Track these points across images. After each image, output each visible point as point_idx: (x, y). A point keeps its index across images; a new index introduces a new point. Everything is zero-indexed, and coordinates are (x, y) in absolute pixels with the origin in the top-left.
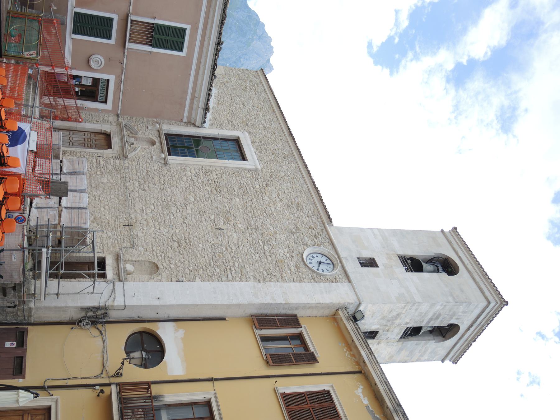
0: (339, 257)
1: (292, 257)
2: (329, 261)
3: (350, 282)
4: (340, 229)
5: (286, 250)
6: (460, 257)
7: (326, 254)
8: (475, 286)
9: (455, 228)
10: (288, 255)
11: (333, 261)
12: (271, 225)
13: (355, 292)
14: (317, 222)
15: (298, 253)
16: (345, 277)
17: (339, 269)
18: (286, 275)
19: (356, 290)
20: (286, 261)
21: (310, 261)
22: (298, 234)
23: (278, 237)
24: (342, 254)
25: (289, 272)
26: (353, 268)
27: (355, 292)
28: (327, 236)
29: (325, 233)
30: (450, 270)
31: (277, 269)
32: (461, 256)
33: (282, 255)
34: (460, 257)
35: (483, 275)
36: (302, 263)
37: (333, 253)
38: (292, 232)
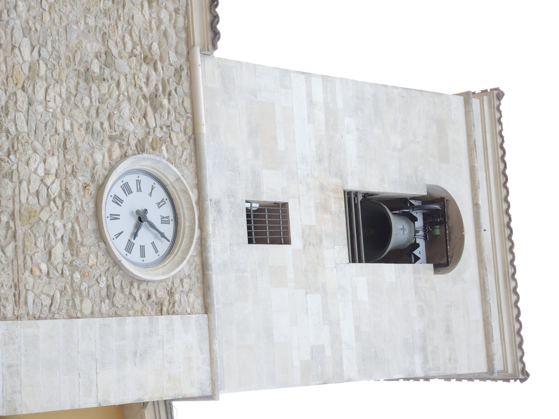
0: (201, 201)
1: (68, 194)
2: (168, 230)
3: (207, 309)
4: (227, 68)
5: (53, 162)
6: (476, 205)
7: (167, 182)
8: (478, 316)
9: (499, 95)
10: (55, 188)
11: (180, 212)
12: (27, 31)
13: (211, 351)
14: (171, 32)
15: (88, 180)
16: (198, 286)
17: (186, 266)
18: (31, 280)
19: (216, 347)
20: (44, 216)
21: (121, 195)
22: (105, 87)
23: (40, 95)
24: (214, 188)
25: (44, 267)
26: (227, 231)
27: (211, 351)
28: (187, 104)
29: (185, 84)
30: (437, 232)
31: (9, 250)
32: (480, 202)
33: (34, 187)
34: (476, 205)
35: (505, 273)
36: (91, 225)
37: (188, 181)
38: (87, 76)
